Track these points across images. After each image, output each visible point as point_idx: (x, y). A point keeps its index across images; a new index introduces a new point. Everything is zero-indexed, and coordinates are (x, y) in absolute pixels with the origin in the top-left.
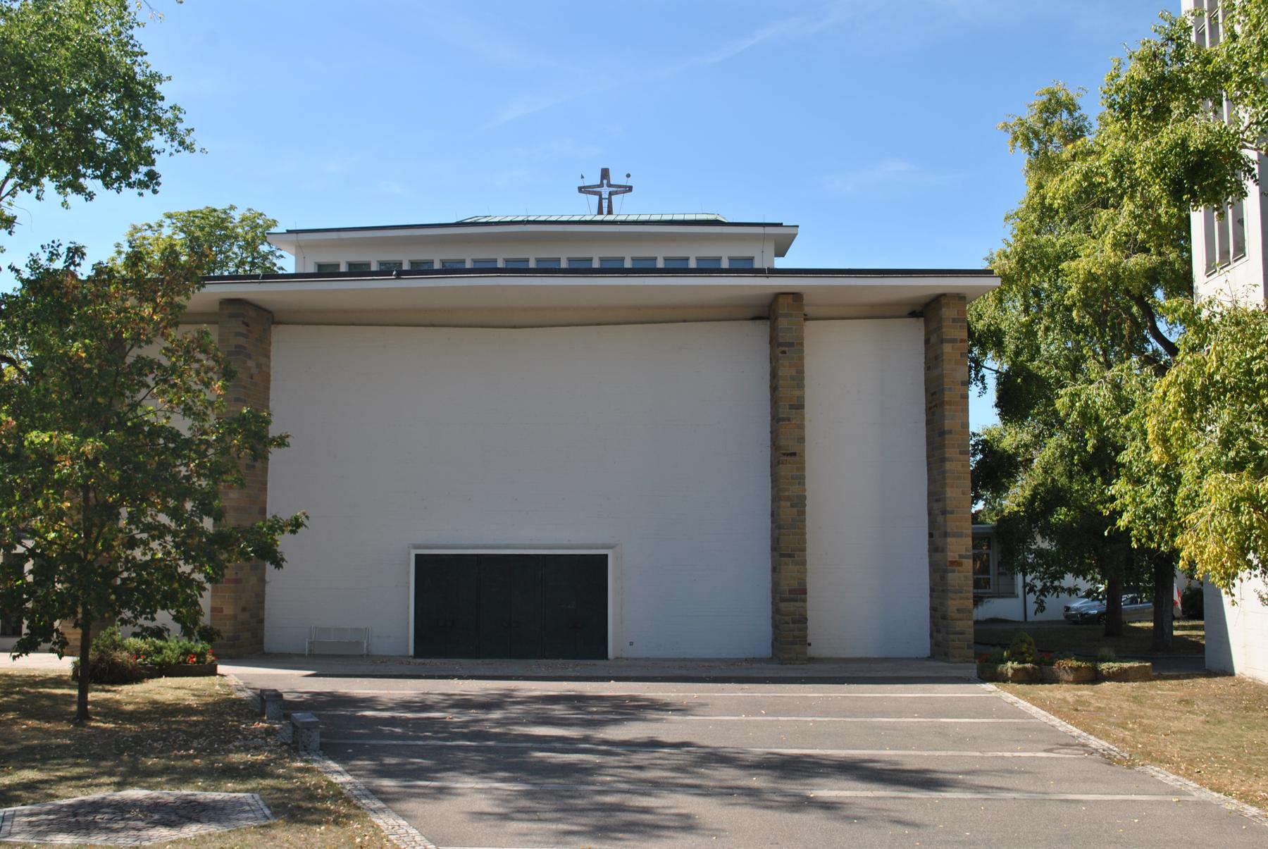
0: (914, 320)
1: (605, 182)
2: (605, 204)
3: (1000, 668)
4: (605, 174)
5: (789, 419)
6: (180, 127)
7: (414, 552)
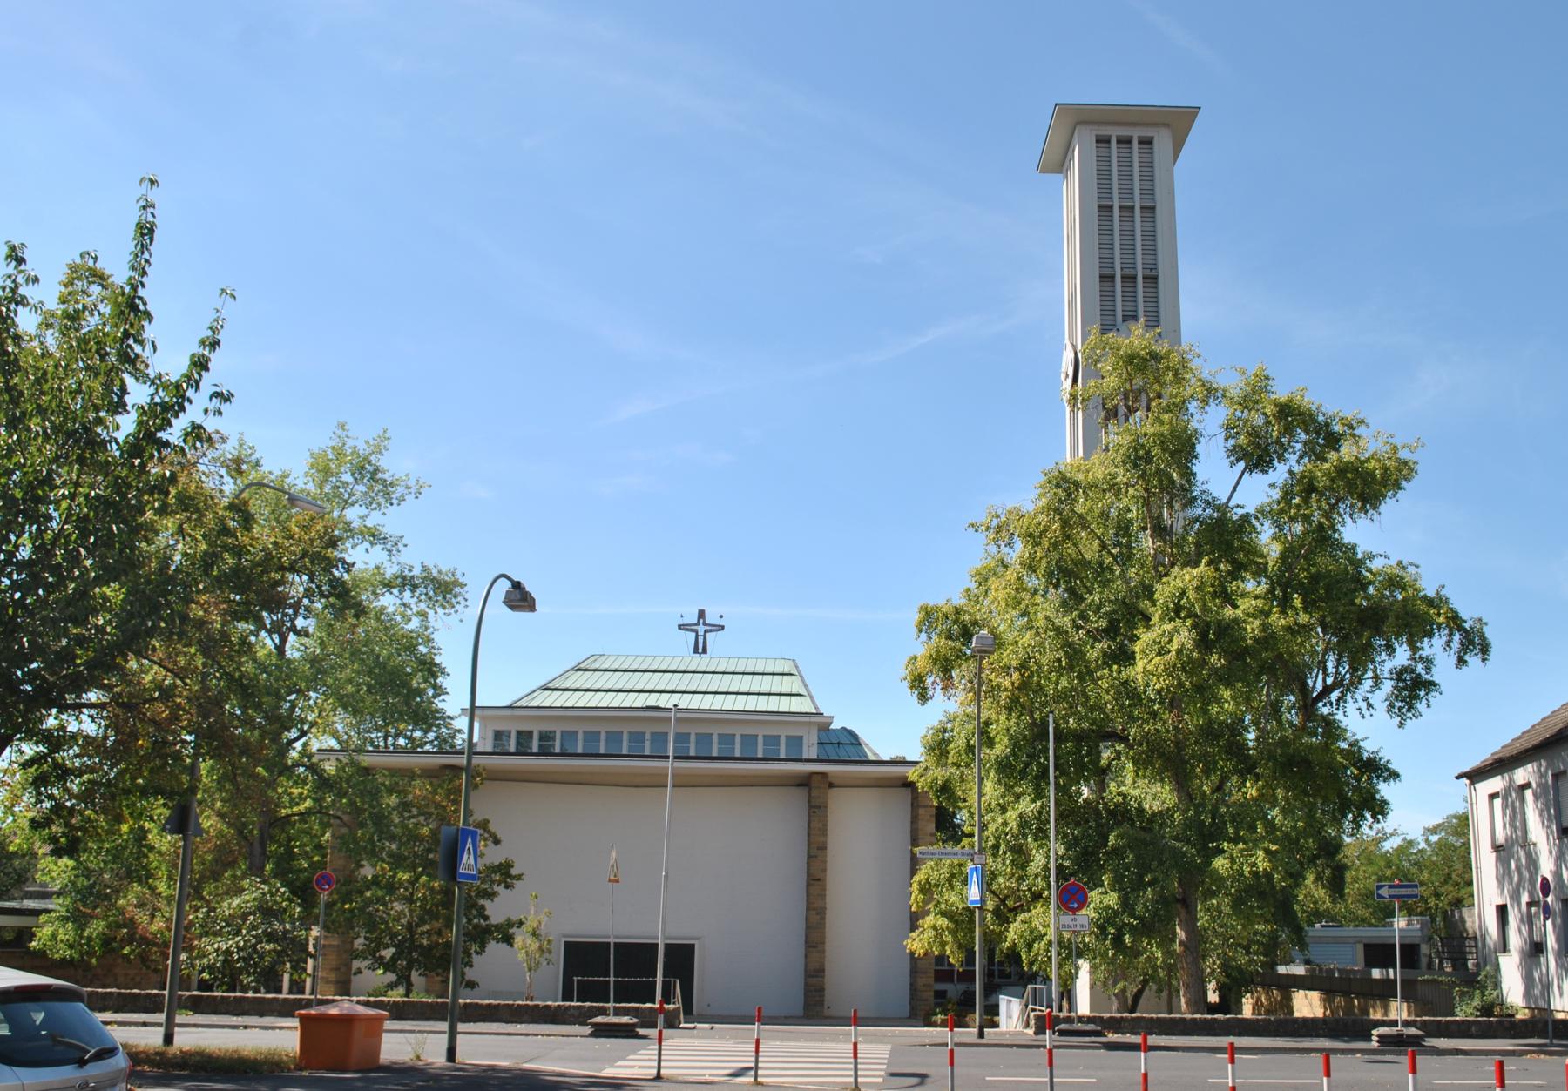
0: (904, 789)
1: (701, 621)
2: (701, 640)
3: (934, 1018)
4: (701, 614)
5: (816, 857)
6: (14, 263)
7: (564, 940)
